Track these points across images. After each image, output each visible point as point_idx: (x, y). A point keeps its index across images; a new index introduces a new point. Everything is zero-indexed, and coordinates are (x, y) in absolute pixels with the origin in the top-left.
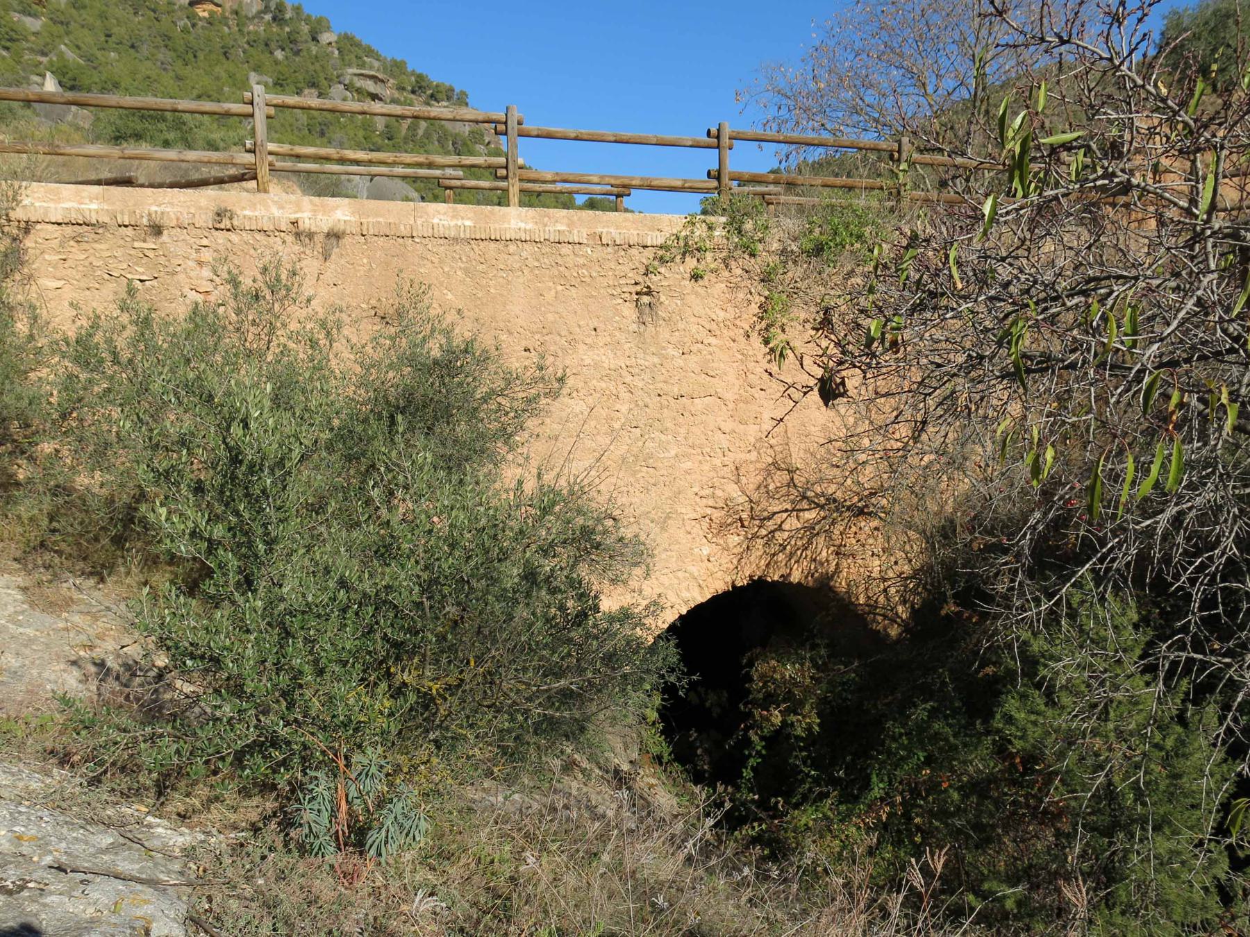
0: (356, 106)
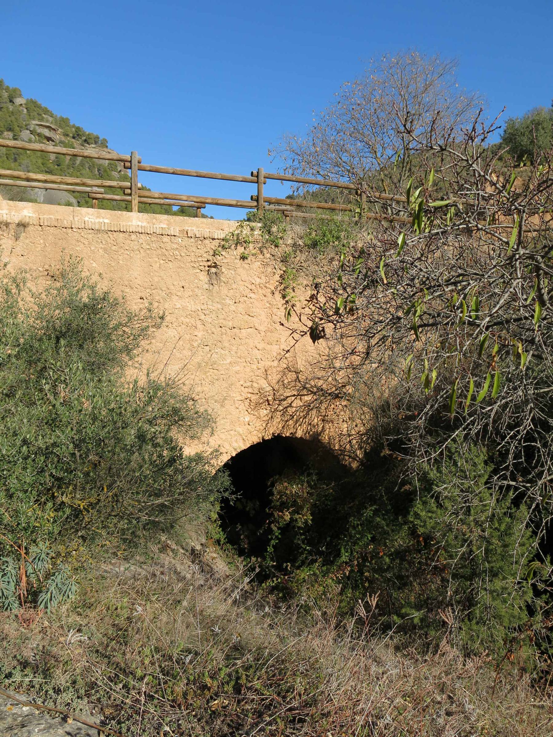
0: (37, 146)
